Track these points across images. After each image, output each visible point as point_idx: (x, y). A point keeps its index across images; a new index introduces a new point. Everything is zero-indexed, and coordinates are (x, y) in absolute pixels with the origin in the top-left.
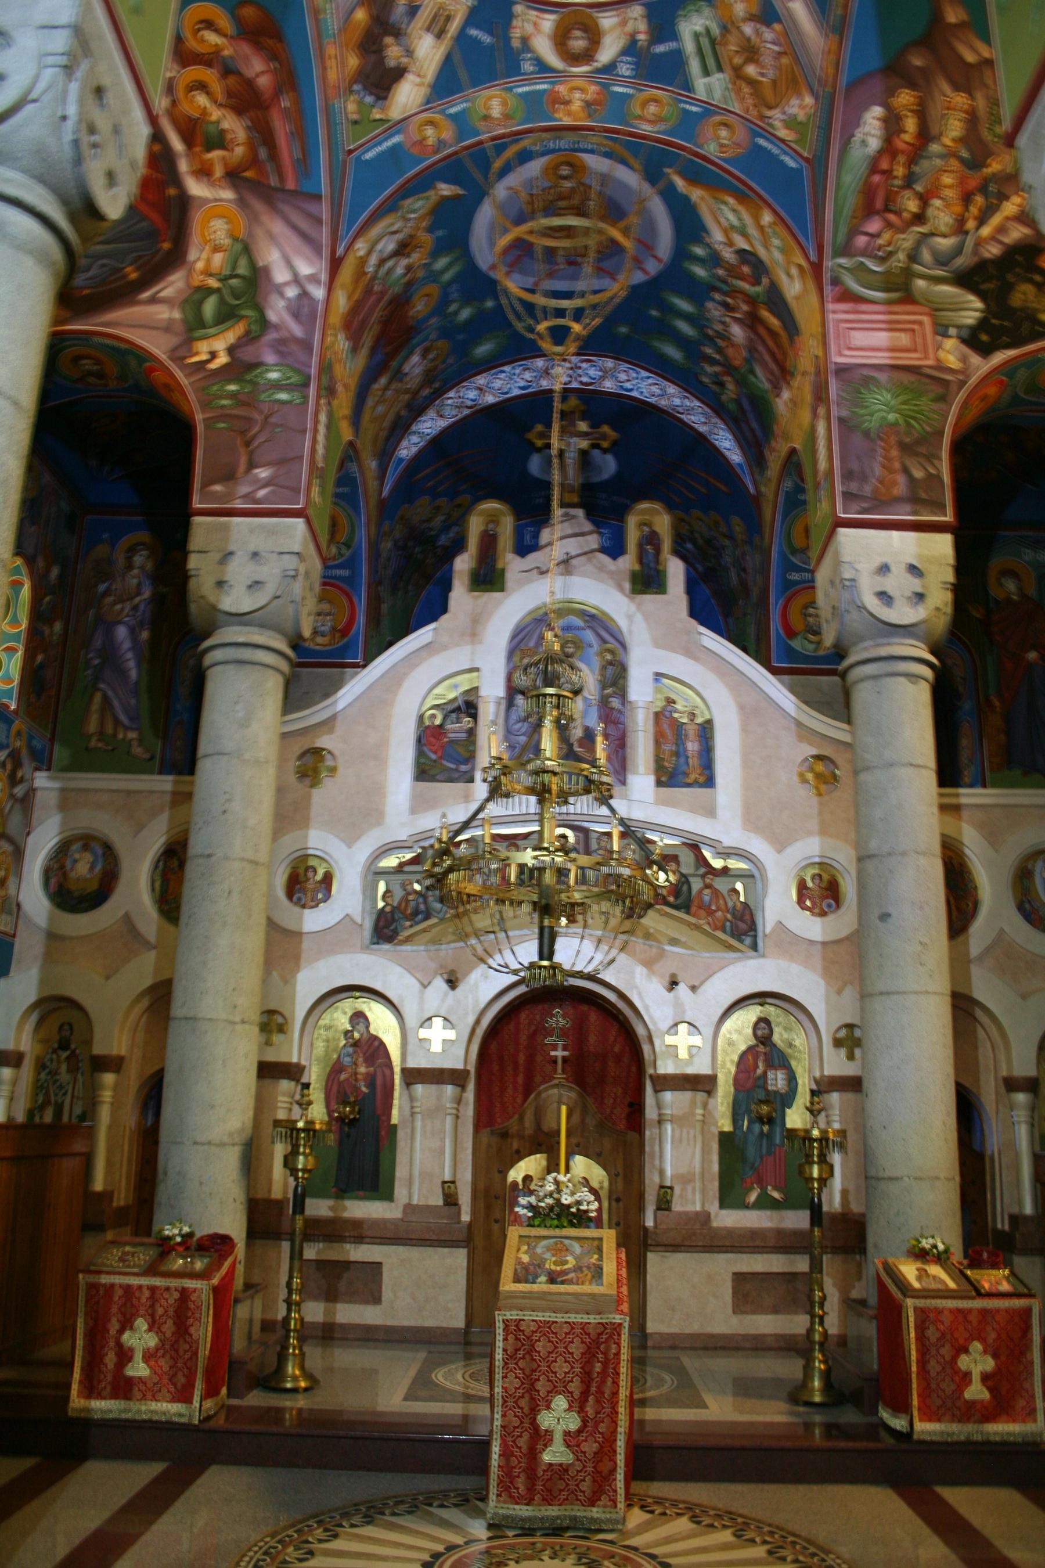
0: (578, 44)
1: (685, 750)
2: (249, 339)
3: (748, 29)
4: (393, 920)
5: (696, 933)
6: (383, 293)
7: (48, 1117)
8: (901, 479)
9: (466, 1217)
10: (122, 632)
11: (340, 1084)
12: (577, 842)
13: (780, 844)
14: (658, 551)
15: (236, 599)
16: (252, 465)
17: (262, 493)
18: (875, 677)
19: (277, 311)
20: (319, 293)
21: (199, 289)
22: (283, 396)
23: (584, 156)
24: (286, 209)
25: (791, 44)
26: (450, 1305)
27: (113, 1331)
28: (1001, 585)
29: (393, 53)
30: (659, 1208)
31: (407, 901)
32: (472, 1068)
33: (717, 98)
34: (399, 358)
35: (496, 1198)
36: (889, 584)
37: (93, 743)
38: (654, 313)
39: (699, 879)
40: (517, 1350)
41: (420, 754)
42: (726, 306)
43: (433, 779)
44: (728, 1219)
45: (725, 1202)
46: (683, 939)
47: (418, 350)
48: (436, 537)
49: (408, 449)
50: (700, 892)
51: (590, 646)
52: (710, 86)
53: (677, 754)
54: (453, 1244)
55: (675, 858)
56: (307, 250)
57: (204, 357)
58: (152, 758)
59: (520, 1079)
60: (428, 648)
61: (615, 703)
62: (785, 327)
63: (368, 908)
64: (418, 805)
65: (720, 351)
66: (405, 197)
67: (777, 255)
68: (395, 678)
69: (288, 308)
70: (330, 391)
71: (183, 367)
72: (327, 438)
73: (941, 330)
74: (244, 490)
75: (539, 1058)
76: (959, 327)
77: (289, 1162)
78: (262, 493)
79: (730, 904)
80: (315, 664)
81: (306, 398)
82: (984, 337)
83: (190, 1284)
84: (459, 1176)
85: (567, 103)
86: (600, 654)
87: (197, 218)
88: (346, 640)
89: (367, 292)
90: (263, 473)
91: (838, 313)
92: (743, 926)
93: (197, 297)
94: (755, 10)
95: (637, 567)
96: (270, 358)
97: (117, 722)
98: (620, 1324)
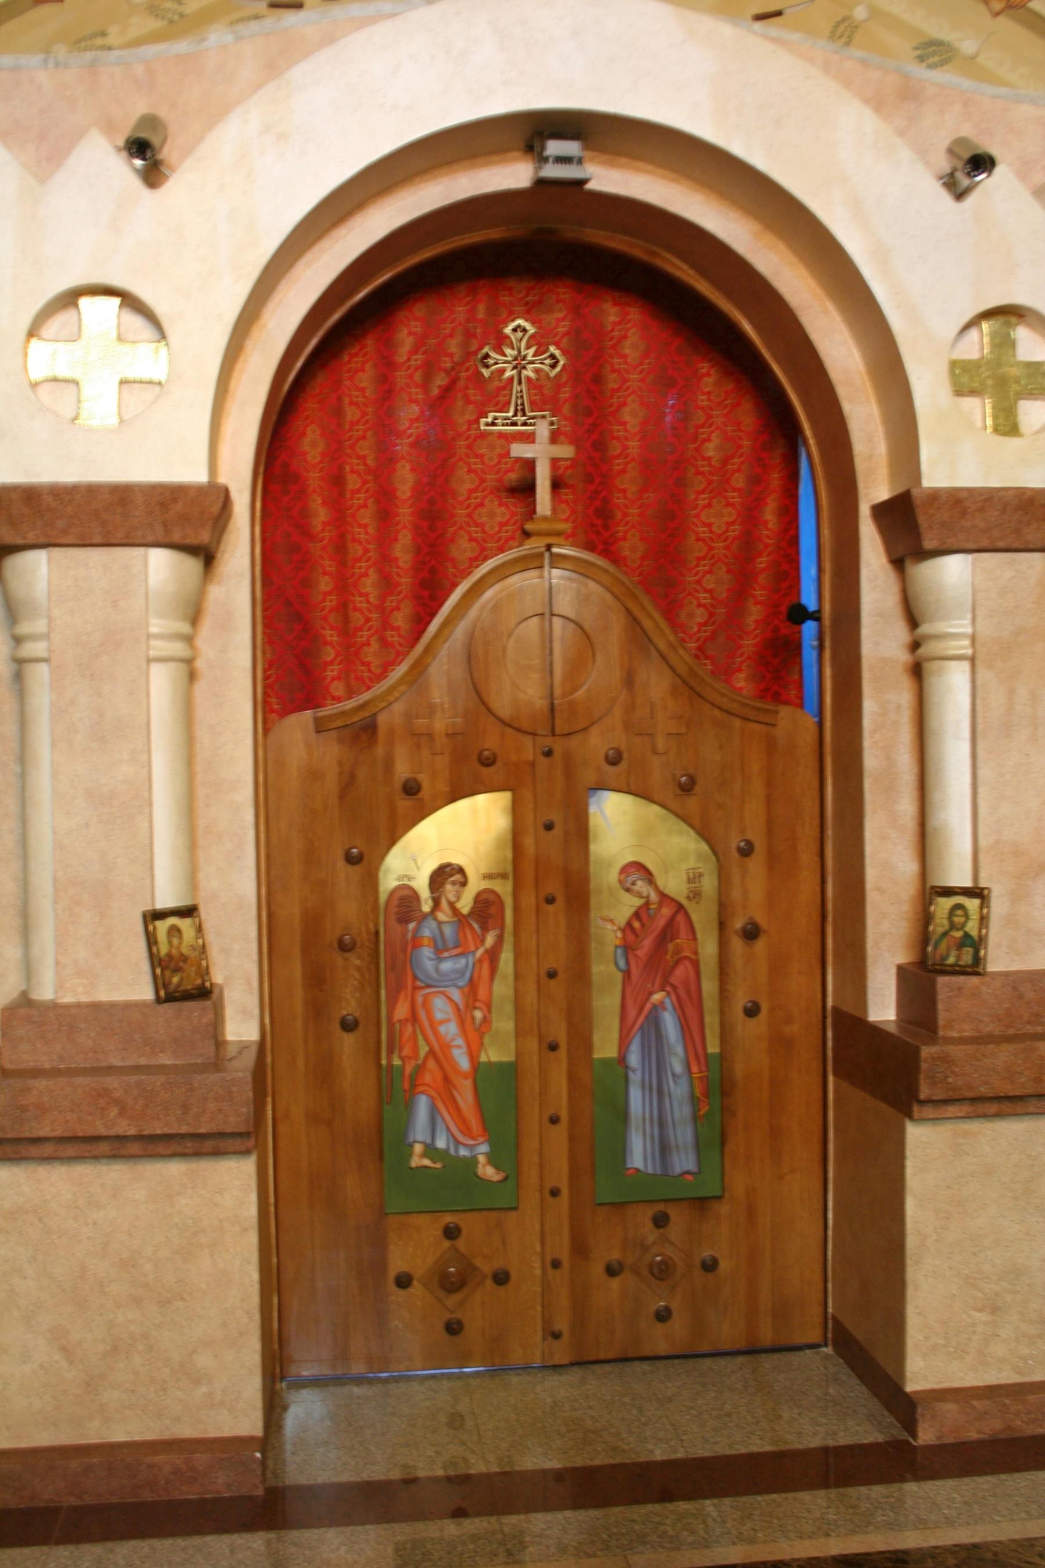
9: (242, 1025)
26: (204, 1361)
32: (238, 472)
35: (344, 947)
46: (968, 46)
59: (403, 550)
84: (210, 882)
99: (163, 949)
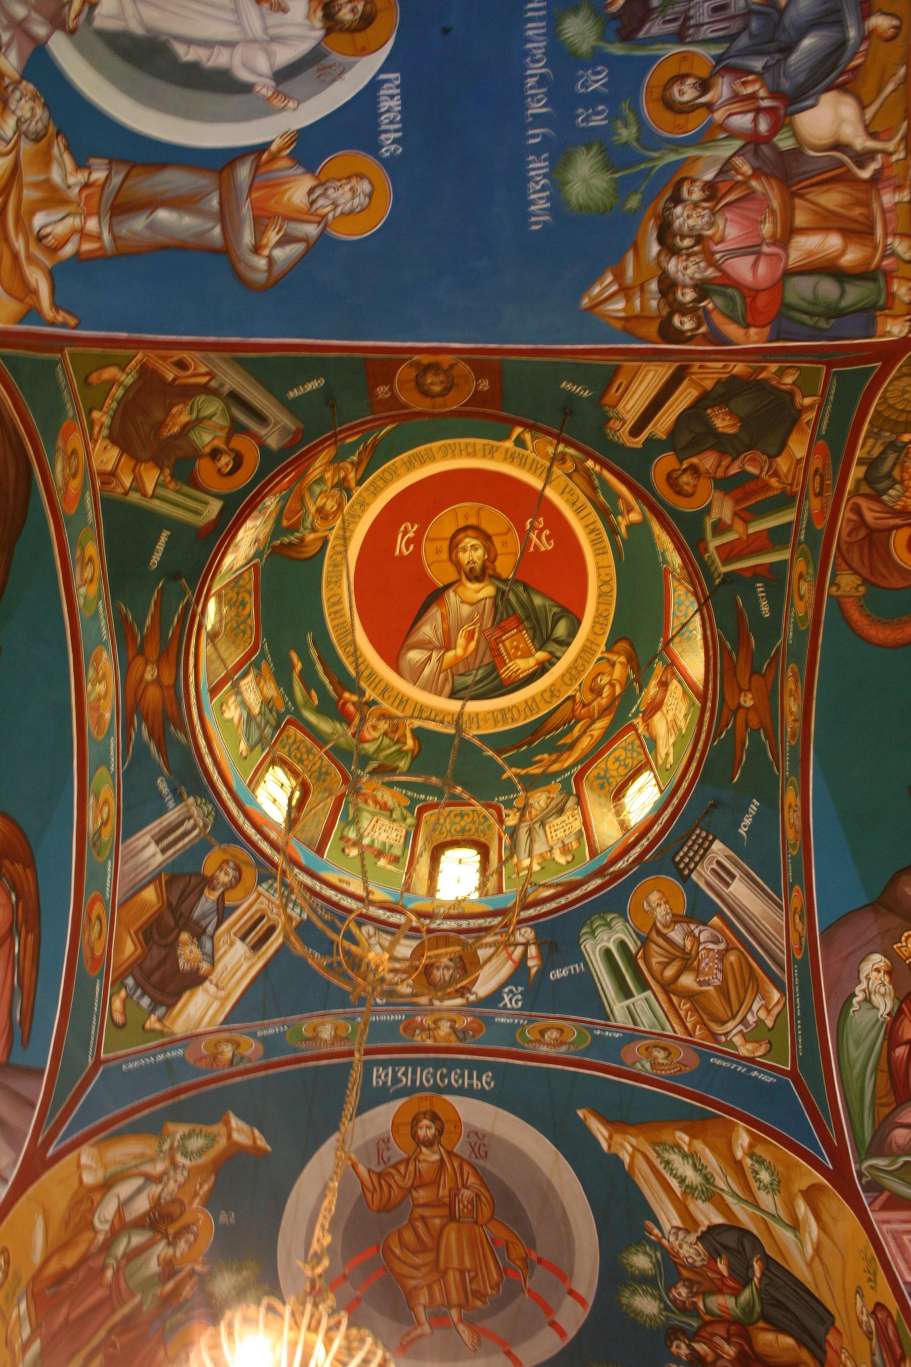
3: (676, 934)
23: (453, 1100)
25: (739, 934)
29: (188, 953)
33: (646, 1022)
52: (635, 1009)
67: (767, 1200)
94: (682, 910)
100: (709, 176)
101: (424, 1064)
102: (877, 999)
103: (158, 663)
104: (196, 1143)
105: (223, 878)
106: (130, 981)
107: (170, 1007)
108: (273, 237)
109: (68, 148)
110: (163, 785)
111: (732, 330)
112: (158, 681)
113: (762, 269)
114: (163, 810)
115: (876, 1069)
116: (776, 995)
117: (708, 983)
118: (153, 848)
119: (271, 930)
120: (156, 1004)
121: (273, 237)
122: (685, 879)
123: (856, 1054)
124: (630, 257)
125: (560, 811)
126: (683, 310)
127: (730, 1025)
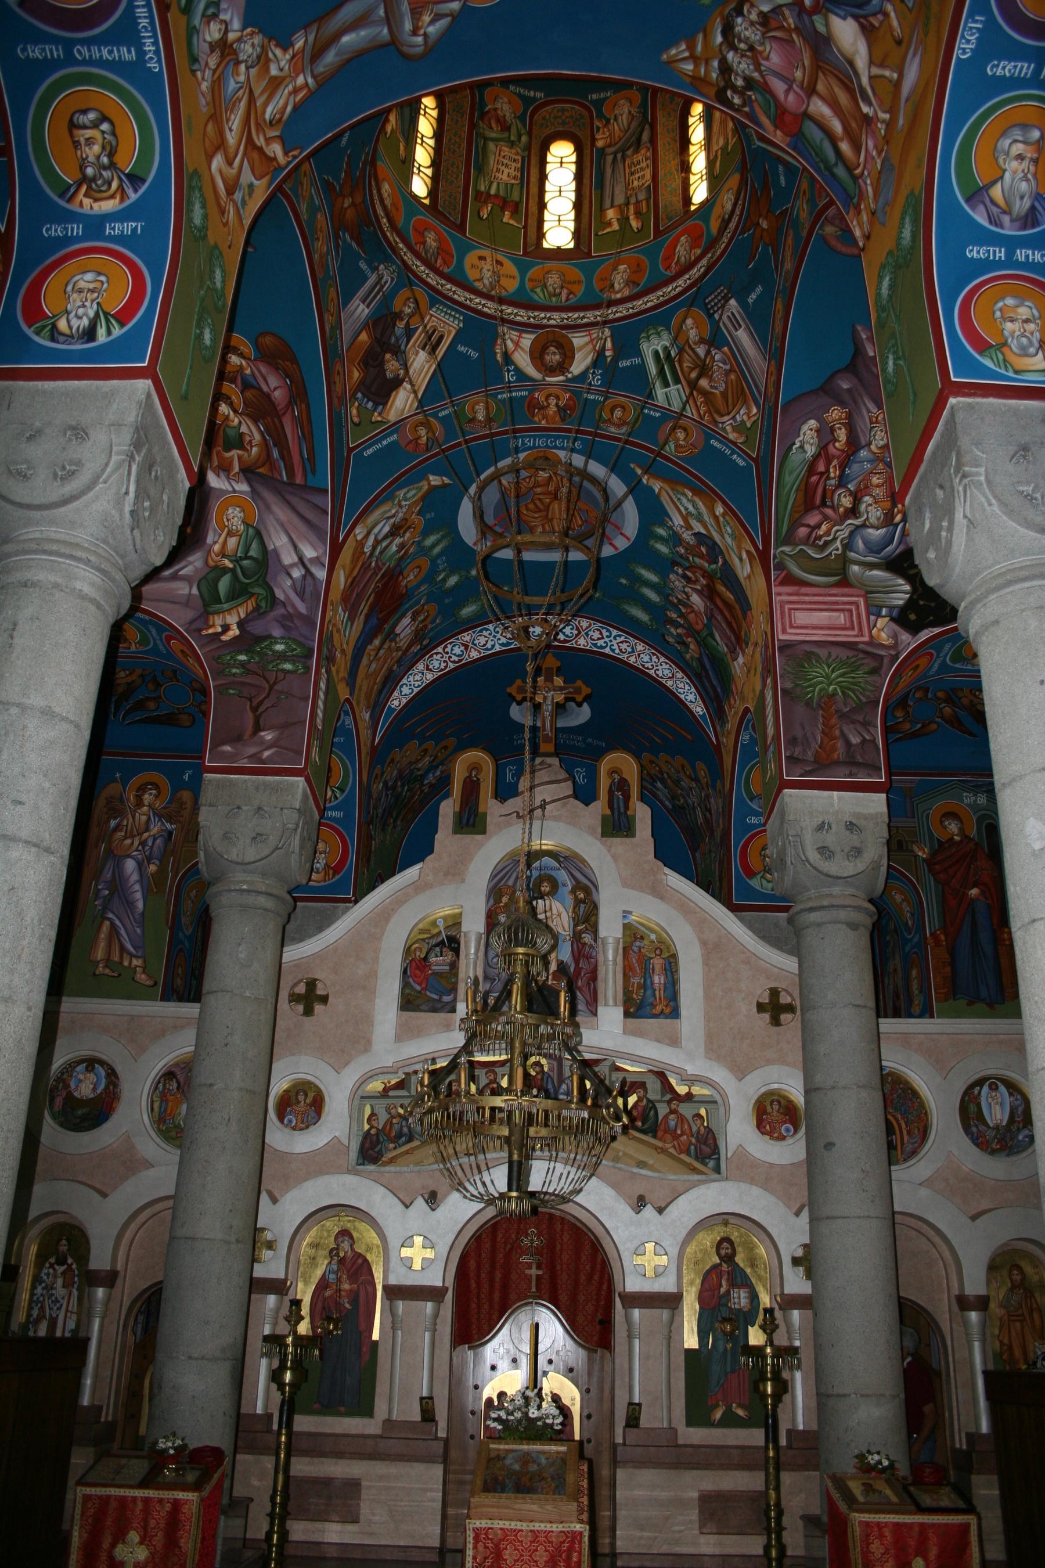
0: (553, 357)
1: (652, 983)
2: (258, 613)
3: (701, 351)
4: (378, 1142)
5: (662, 1156)
6: (378, 567)
7: (42, 1332)
8: (840, 744)
10: (130, 865)
11: (325, 1299)
12: (551, 1069)
13: (740, 1072)
14: (627, 798)
15: (243, 850)
16: (257, 728)
17: (266, 754)
18: (819, 925)
19: (284, 589)
20: (321, 574)
21: (216, 567)
22: (288, 666)
24: (294, 500)
25: (737, 361)
27: (106, 1545)
28: (945, 827)
29: (392, 366)
30: (628, 1425)
31: (392, 1124)
32: (450, 1283)
33: (676, 406)
34: (391, 622)
36: (830, 839)
37: (100, 969)
38: (624, 581)
39: (665, 1105)
40: (486, 1558)
41: (405, 985)
42: (685, 576)
43: (417, 1009)
44: (697, 1435)
45: (690, 1422)
46: (651, 1162)
47: (409, 614)
48: (423, 777)
49: (398, 700)
50: (666, 1117)
51: (564, 885)
52: (669, 396)
53: (644, 986)
54: (427, 1459)
55: (643, 1085)
56: (314, 539)
57: (220, 630)
58: (156, 984)
59: (497, 1296)
60: (419, 887)
61: (587, 938)
62: (738, 600)
63: (355, 1129)
64: (403, 1034)
65: (681, 615)
66: (400, 488)
67: (729, 540)
68: (384, 916)
69: (294, 587)
70: (331, 659)
71: (199, 637)
72: (326, 694)
73: (874, 610)
74: (252, 750)
75: (514, 1276)
76: (891, 608)
77: (276, 1377)
78: (266, 754)
79: (694, 1129)
80: (309, 901)
81: (308, 669)
82: (913, 617)
83: (181, 1495)
85: (542, 408)
86: (573, 891)
87: (215, 508)
88: (337, 877)
89: (363, 566)
90: (268, 736)
91: (782, 595)
92: (706, 1150)
93: (213, 575)
94: (707, 336)
95: (608, 812)
96: (277, 632)
97: (123, 948)
98: (581, 1533)
99: (555, 539)
100: (765, 8)
101: (540, 437)
102: (807, 447)
103: (351, 195)
104: (410, 495)
105: (407, 310)
106: (359, 395)
107: (385, 404)
108: (427, 19)
109: (277, 45)
110: (363, 265)
111: (764, 120)
112: (353, 204)
113: (791, 97)
114: (366, 279)
115: (797, 490)
116: (755, 410)
117: (716, 388)
118: (362, 306)
119: (441, 337)
120: (376, 405)
121: (427, 19)
122: (710, 316)
123: (788, 479)
124: (700, 37)
125: (638, 145)
126: (735, 89)
127: (726, 418)
